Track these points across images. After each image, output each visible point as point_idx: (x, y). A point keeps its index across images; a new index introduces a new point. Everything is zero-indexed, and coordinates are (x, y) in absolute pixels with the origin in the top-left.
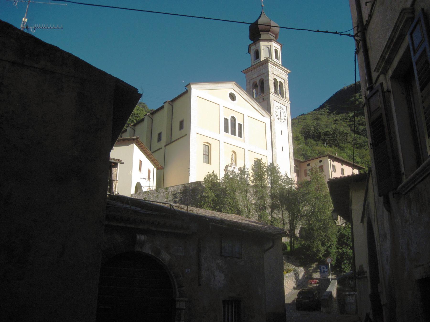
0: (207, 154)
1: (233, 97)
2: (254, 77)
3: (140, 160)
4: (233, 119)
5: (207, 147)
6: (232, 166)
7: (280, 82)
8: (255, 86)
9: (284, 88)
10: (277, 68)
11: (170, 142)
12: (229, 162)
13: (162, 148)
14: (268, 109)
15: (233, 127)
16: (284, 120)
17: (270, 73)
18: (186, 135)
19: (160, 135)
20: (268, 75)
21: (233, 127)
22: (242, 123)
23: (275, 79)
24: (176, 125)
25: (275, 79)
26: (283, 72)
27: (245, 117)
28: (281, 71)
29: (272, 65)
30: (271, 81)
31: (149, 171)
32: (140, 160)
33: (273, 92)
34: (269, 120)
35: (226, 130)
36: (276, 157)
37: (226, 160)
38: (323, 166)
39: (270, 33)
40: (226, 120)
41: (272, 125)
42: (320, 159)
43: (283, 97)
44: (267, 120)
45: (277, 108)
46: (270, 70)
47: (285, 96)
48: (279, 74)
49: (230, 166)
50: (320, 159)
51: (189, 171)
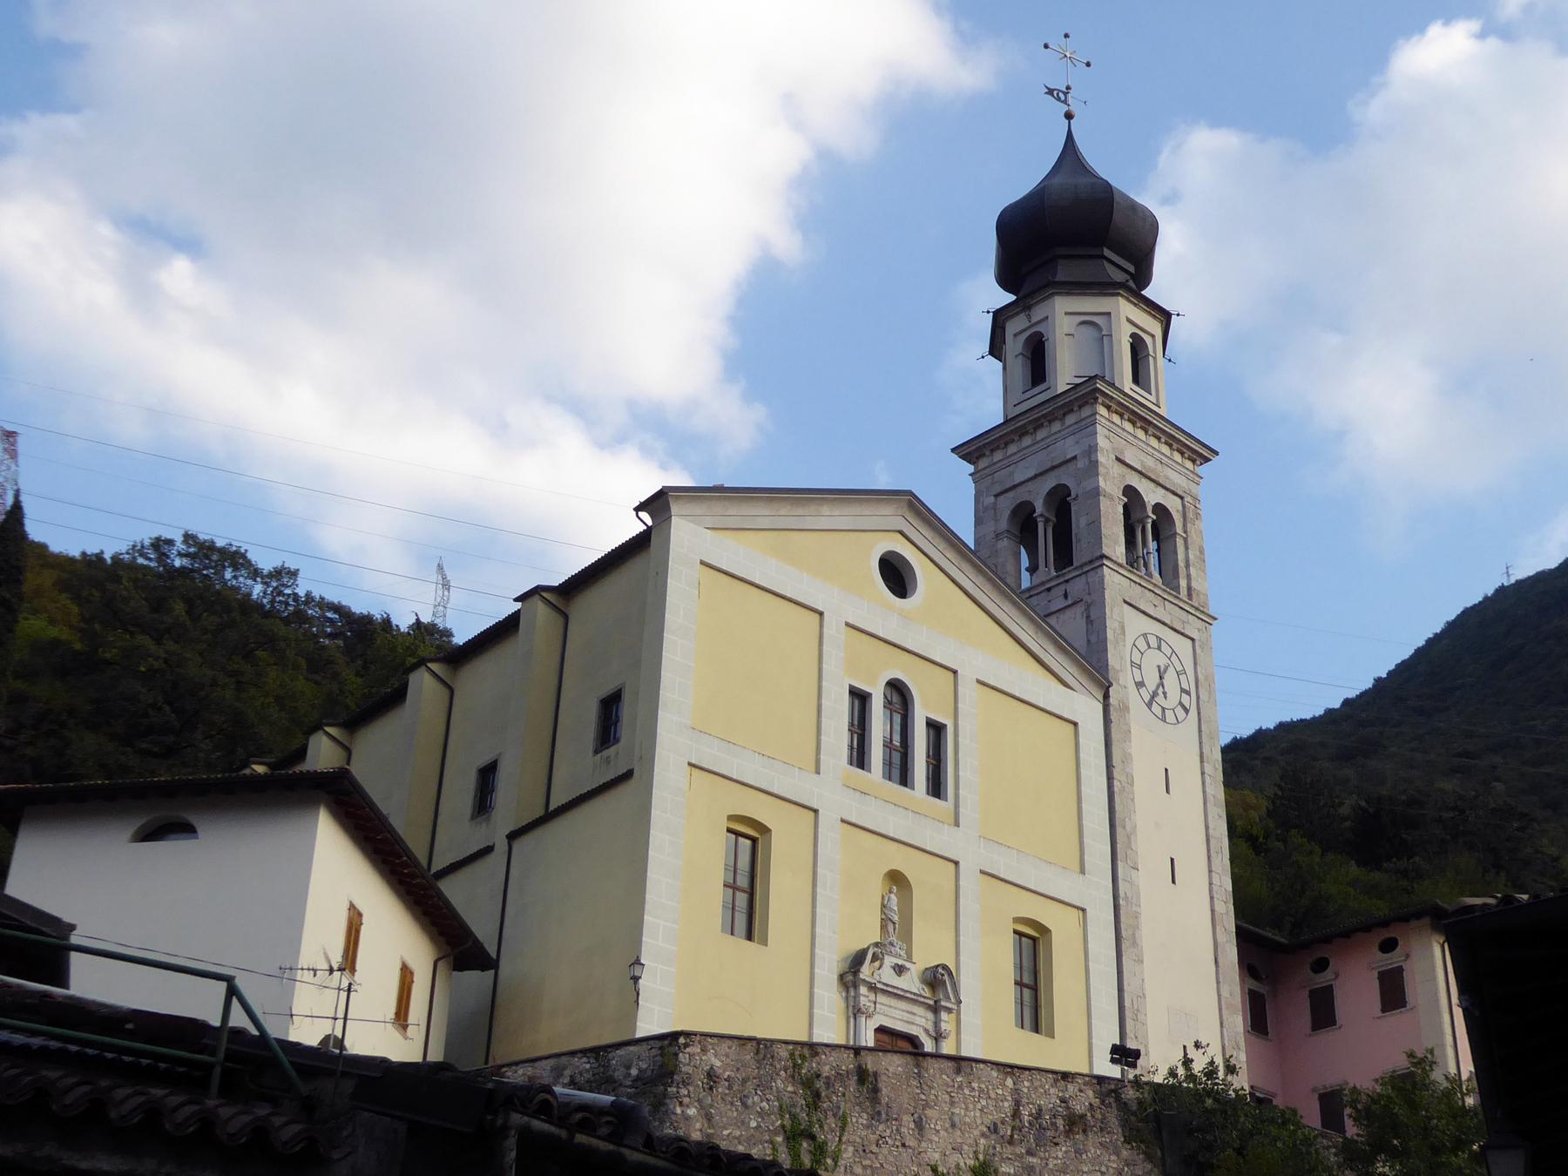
0: (743, 882)
1: (896, 576)
2: (1018, 478)
3: (352, 907)
4: (899, 692)
5: (745, 844)
6: (889, 961)
7: (1160, 509)
8: (1024, 525)
9: (1180, 542)
10: (1140, 434)
11: (539, 812)
12: (870, 934)
13: (488, 850)
14: (1093, 663)
15: (901, 739)
16: (1181, 713)
17: (1105, 459)
18: (629, 775)
19: (487, 775)
20: (1093, 467)
21: (901, 739)
22: (948, 721)
23: (1130, 491)
24: (581, 717)
25: (1130, 491)
26: (1177, 457)
27: (968, 690)
28: (1165, 449)
29: (1116, 419)
30: (1111, 498)
31: (406, 975)
32: (352, 907)
33: (1122, 560)
34: (1100, 707)
35: (860, 758)
36: (1136, 916)
37: (850, 923)
38: (1400, 970)
39: (1107, 252)
40: (860, 698)
41: (1115, 735)
42: (1387, 934)
43: (1177, 588)
44: (1086, 708)
45: (1142, 644)
46: (1102, 442)
47: (1183, 583)
48: (1150, 462)
49: (875, 958)
50: (1387, 934)
51: (636, 979)
